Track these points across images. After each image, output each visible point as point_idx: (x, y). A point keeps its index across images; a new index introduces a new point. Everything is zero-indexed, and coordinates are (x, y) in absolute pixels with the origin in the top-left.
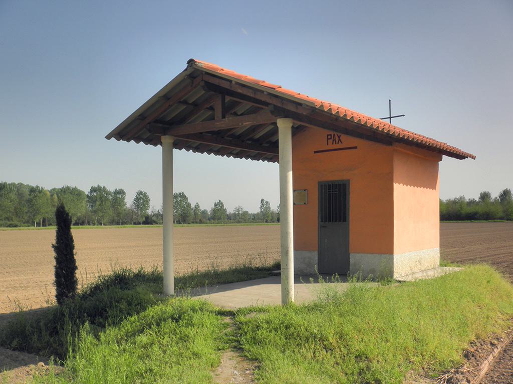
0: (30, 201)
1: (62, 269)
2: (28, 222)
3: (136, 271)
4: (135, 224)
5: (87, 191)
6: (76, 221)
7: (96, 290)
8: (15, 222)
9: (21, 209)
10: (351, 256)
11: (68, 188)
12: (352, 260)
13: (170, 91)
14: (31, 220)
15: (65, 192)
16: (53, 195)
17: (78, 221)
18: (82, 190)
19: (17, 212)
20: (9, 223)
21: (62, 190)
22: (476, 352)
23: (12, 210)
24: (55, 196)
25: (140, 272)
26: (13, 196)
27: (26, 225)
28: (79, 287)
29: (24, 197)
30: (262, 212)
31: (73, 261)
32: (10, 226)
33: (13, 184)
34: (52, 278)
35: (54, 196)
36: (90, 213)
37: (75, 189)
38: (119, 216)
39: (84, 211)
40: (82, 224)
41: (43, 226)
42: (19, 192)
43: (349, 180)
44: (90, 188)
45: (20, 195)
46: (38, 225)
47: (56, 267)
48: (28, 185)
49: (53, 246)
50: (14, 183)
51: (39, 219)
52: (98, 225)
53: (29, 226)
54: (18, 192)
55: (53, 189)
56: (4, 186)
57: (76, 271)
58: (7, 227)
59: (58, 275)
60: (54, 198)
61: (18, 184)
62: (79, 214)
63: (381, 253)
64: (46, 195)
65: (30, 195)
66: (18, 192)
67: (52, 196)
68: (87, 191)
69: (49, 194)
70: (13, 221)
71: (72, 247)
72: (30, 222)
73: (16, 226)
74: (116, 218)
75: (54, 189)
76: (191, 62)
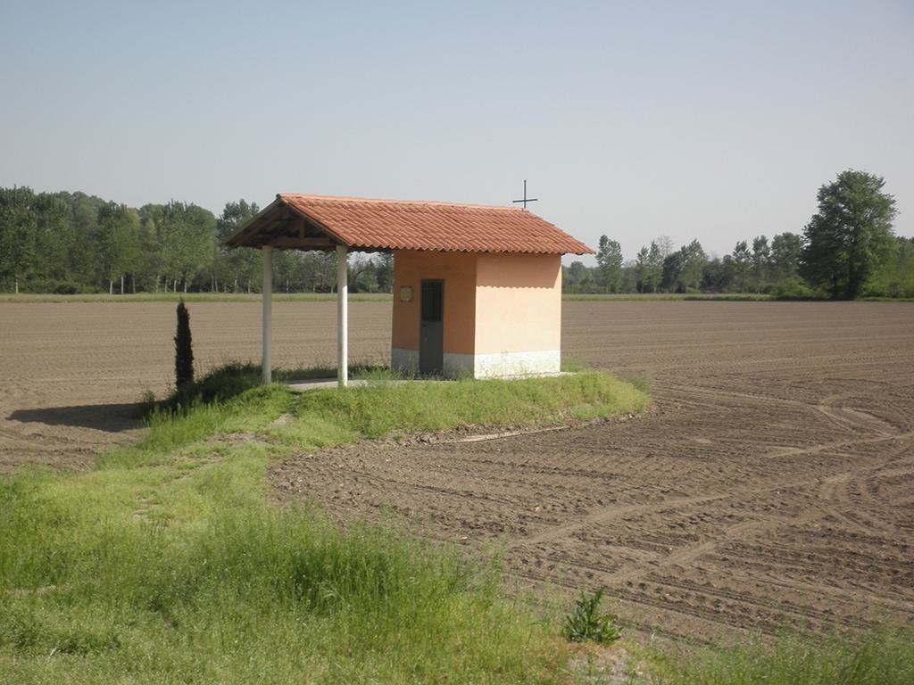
0: (100, 236)
1: (181, 359)
2: (94, 283)
3: (244, 364)
4: (319, 290)
5: (218, 213)
6: (194, 281)
7: (209, 379)
8: (70, 282)
9: (81, 254)
10: (445, 355)
11: (178, 206)
12: (444, 360)
13: (269, 212)
14: (101, 277)
15: (171, 216)
16: (147, 220)
17: (197, 283)
18: (209, 210)
19: (75, 261)
20: (58, 284)
21: (165, 213)
22: (793, 513)
23: (64, 254)
24: (151, 224)
25: (248, 365)
26: (65, 224)
27: (92, 288)
28: (195, 376)
29: (87, 224)
30: (602, 266)
31: (189, 331)
32: (61, 290)
33: (64, 195)
34: (173, 366)
35: (147, 224)
36: (223, 265)
37: (193, 209)
38: (285, 271)
39: (212, 258)
40: (207, 288)
41: (127, 291)
42: (77, 212)
43: (443, 280)
44: (225, 207)
45: (79, 221)
46: (117, 290)
47: (177, 357)
48: (95, 197)
49: (175, 339)
50: (66, 193)
51: (116, 276)
52: (239, 292)
53: (97, 292)
54: (74, 213)
55: (146, 207)
56: (48, 202)
57: (193, 361)
58: (54, 293)
59: (178, 364)
60: (149, 229)
61: (74, 195)
62: (201, 266)
63: (465, 353)
64: (130, 221)
65: (100, 222)
66: (74, 213)
67: (144, 222)
68: (218, 213)
69: (138, 218)
70: (65, 279)
71: (190, 340)
72: (100, 282)
73: (72, 291)
74: (279, 276)
75: (148, 207)
76: (278, 196)
